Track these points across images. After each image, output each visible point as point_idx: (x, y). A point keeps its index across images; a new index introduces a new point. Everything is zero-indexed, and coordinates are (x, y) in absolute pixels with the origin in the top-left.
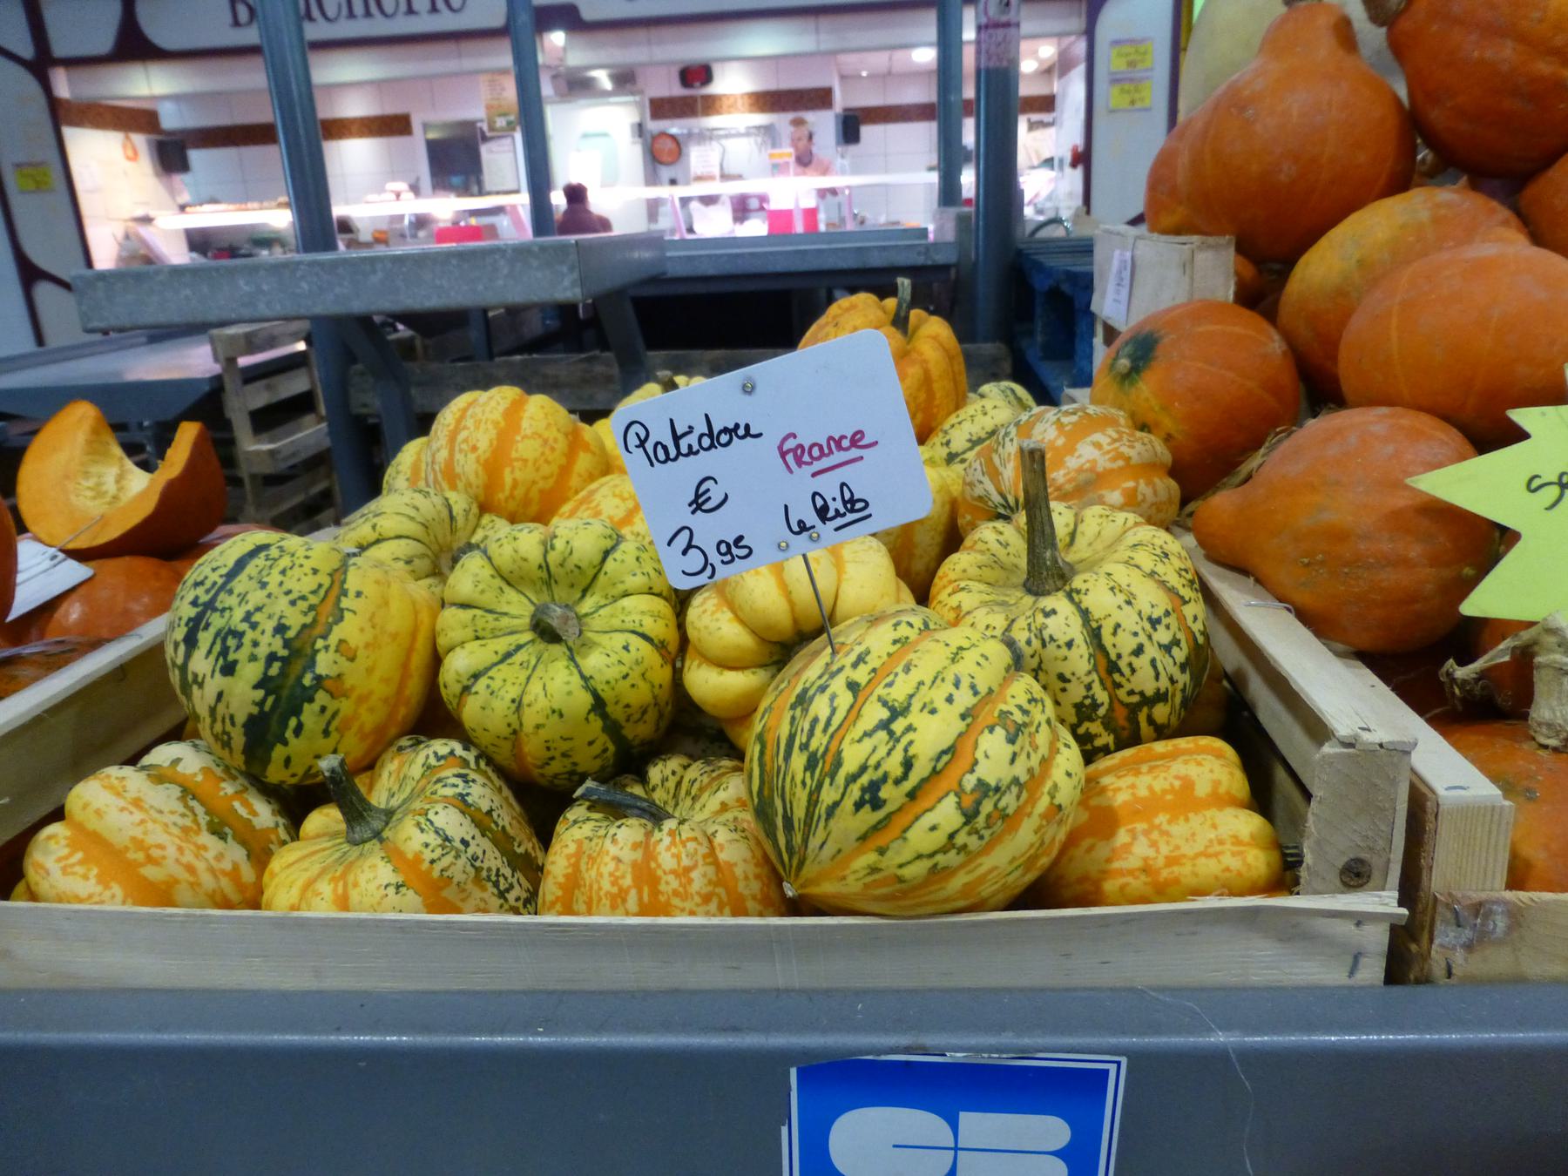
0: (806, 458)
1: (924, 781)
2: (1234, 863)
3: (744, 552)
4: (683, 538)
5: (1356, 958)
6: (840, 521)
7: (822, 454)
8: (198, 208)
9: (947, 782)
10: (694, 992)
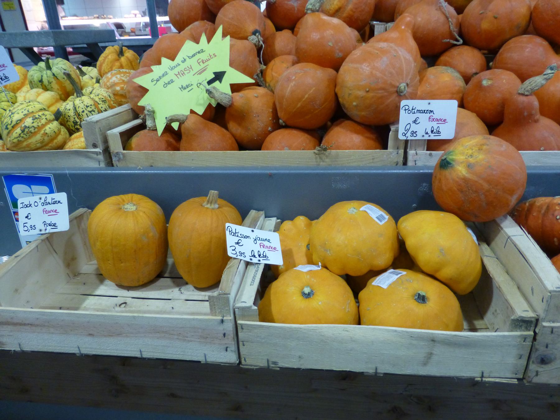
1: (14, 125)
2: (80, 145)
5: (99, 162)
8: (66, 18)
9: (19, 125)
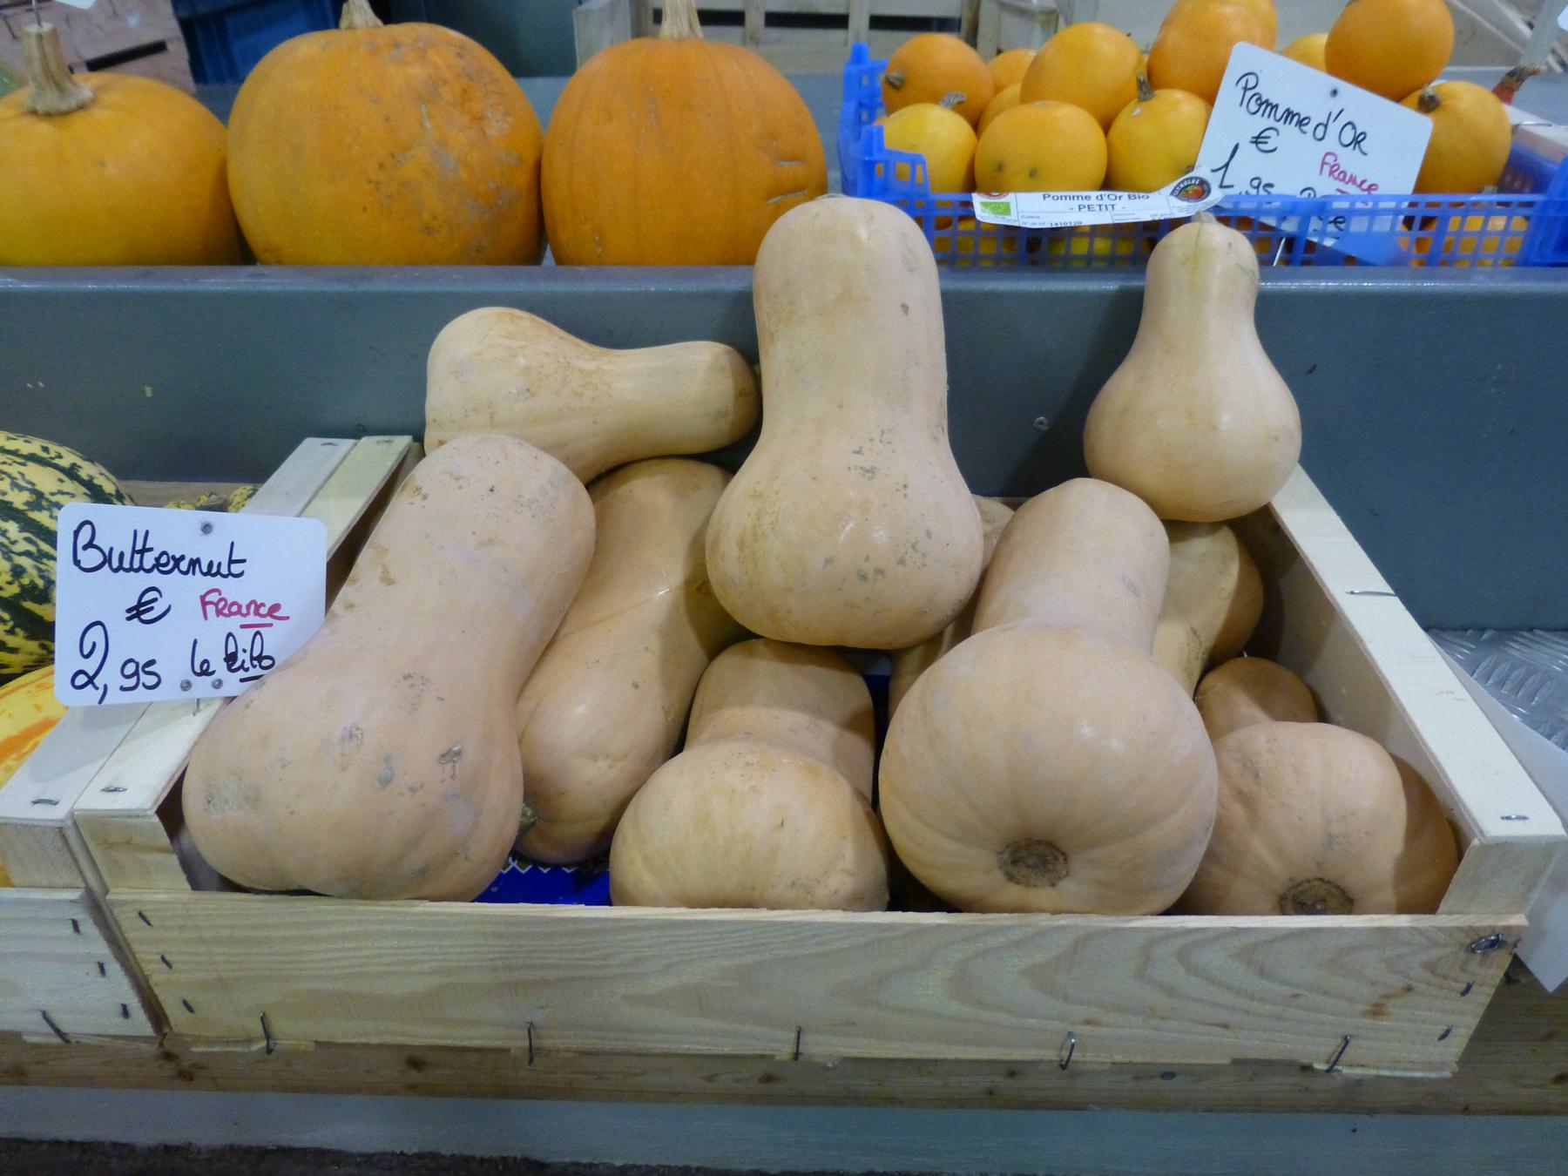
3: (152, 680)
6: (242, 674)
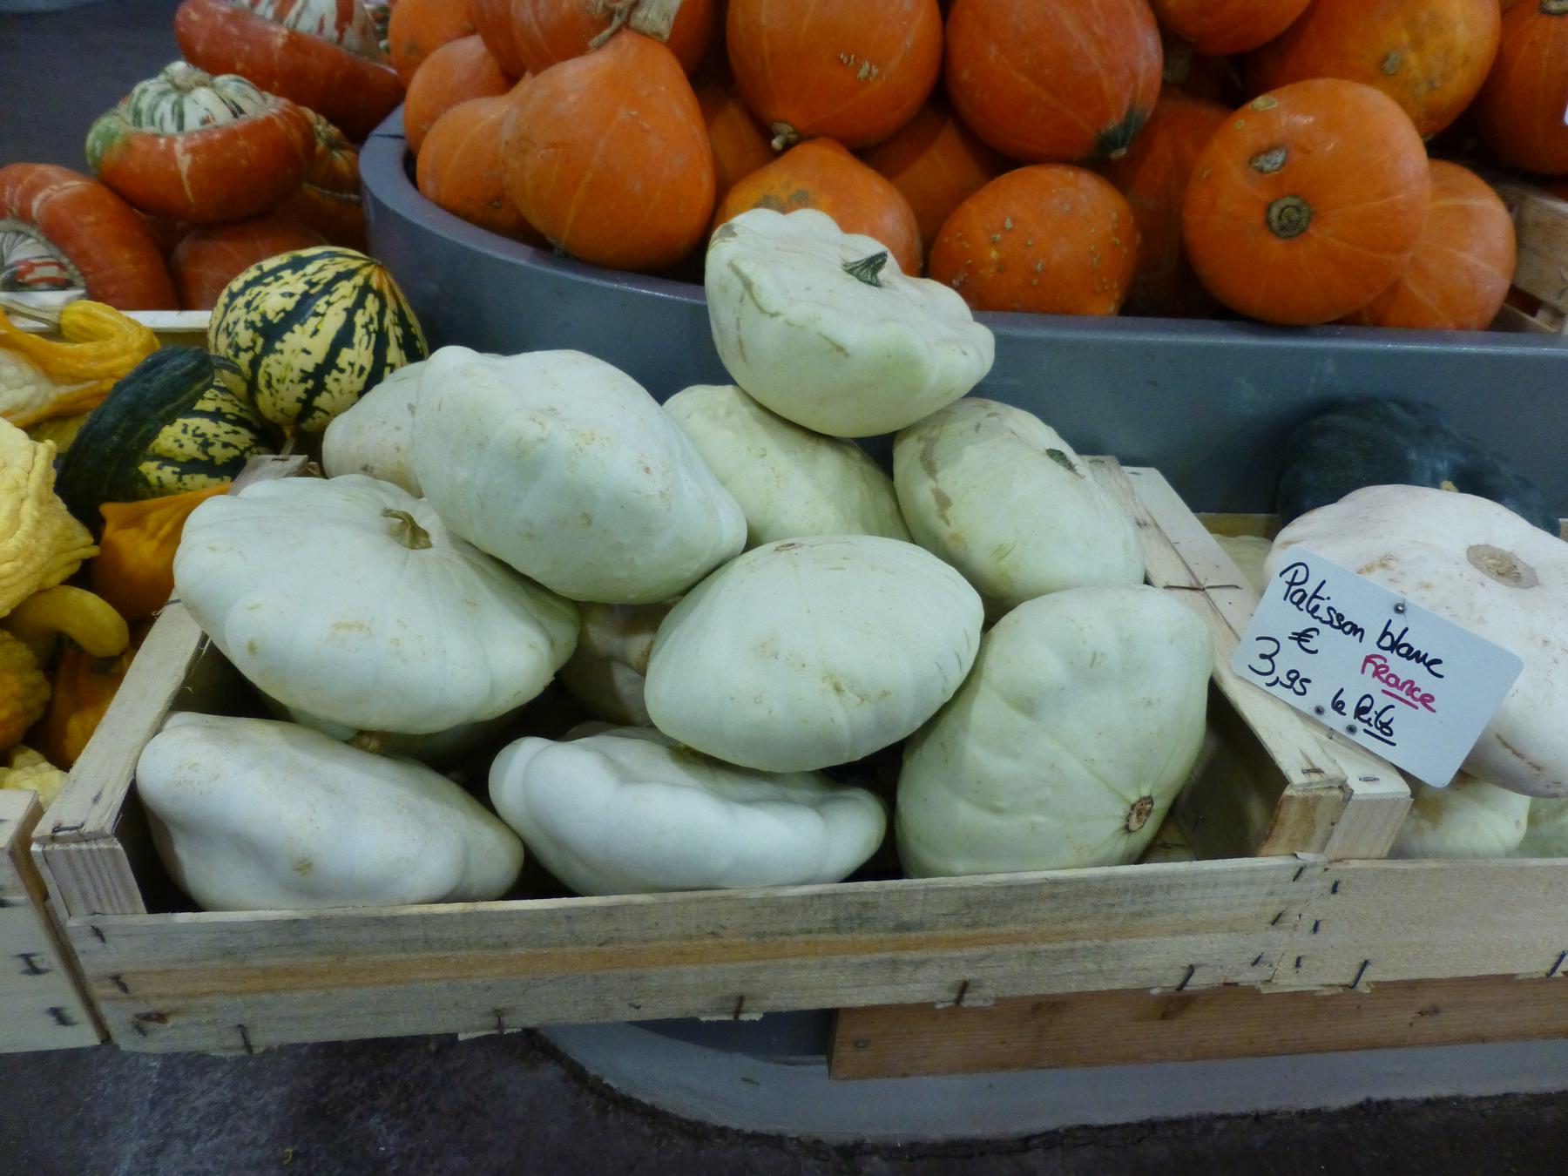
0: (1384, 676)
4: (1269, 648)
7: (1396, 685)
10: (1101, 1129)
